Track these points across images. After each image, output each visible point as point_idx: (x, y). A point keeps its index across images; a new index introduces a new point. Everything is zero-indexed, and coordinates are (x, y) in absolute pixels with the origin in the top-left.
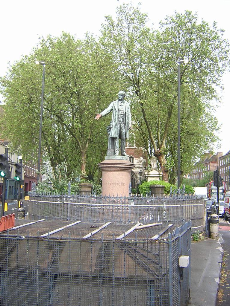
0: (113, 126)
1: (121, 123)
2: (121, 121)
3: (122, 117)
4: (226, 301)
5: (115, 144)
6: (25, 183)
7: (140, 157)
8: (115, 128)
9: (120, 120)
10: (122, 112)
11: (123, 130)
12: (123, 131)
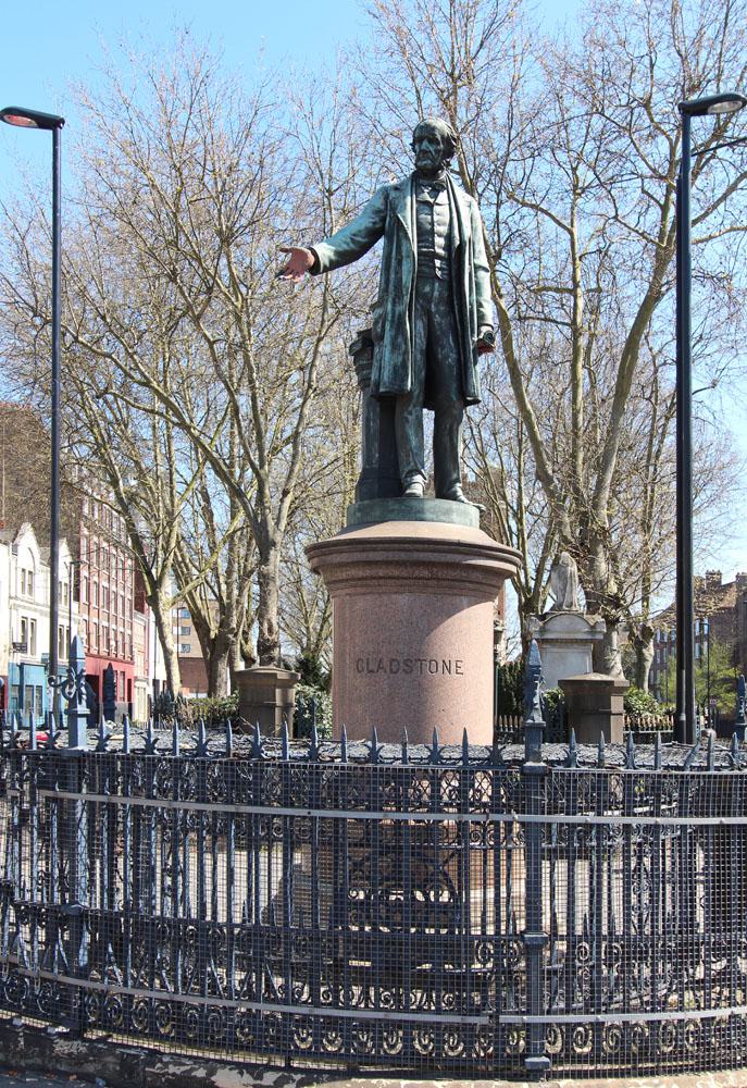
0: (388, 327)
1: (433, 308)
2: (436, 293)
9: (427, 289)
12: (447, 357)
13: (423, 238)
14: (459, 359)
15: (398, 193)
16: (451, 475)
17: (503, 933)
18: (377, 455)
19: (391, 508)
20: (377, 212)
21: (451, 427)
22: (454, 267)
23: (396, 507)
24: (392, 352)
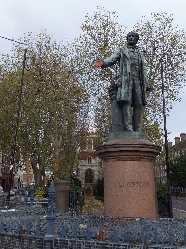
0: (123, 82)
1: (135, 78)
2: (136, 74)
3: (137, 69)
4: (38, 168)
5: (127, 113)
6: (3, 179)
7: (97, 158)
8: (126, 86)
9: (133, 73)
10: (136, 61)
11: (139, 90)
12: (139, 92)
13: (132, 60)
14: (142, 92)
15: (124, 49)
16: (138, 125)
17: (157, 167)
18: (117, 119)
19: (126, 134)
20: (119, 53)
21: (139, 112)
22: (140, 68)
23: (127, 134)
24: (124, 89)
